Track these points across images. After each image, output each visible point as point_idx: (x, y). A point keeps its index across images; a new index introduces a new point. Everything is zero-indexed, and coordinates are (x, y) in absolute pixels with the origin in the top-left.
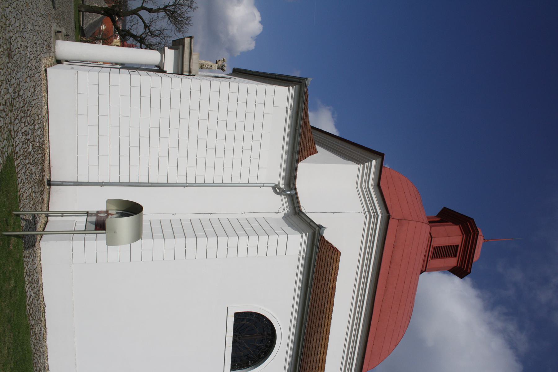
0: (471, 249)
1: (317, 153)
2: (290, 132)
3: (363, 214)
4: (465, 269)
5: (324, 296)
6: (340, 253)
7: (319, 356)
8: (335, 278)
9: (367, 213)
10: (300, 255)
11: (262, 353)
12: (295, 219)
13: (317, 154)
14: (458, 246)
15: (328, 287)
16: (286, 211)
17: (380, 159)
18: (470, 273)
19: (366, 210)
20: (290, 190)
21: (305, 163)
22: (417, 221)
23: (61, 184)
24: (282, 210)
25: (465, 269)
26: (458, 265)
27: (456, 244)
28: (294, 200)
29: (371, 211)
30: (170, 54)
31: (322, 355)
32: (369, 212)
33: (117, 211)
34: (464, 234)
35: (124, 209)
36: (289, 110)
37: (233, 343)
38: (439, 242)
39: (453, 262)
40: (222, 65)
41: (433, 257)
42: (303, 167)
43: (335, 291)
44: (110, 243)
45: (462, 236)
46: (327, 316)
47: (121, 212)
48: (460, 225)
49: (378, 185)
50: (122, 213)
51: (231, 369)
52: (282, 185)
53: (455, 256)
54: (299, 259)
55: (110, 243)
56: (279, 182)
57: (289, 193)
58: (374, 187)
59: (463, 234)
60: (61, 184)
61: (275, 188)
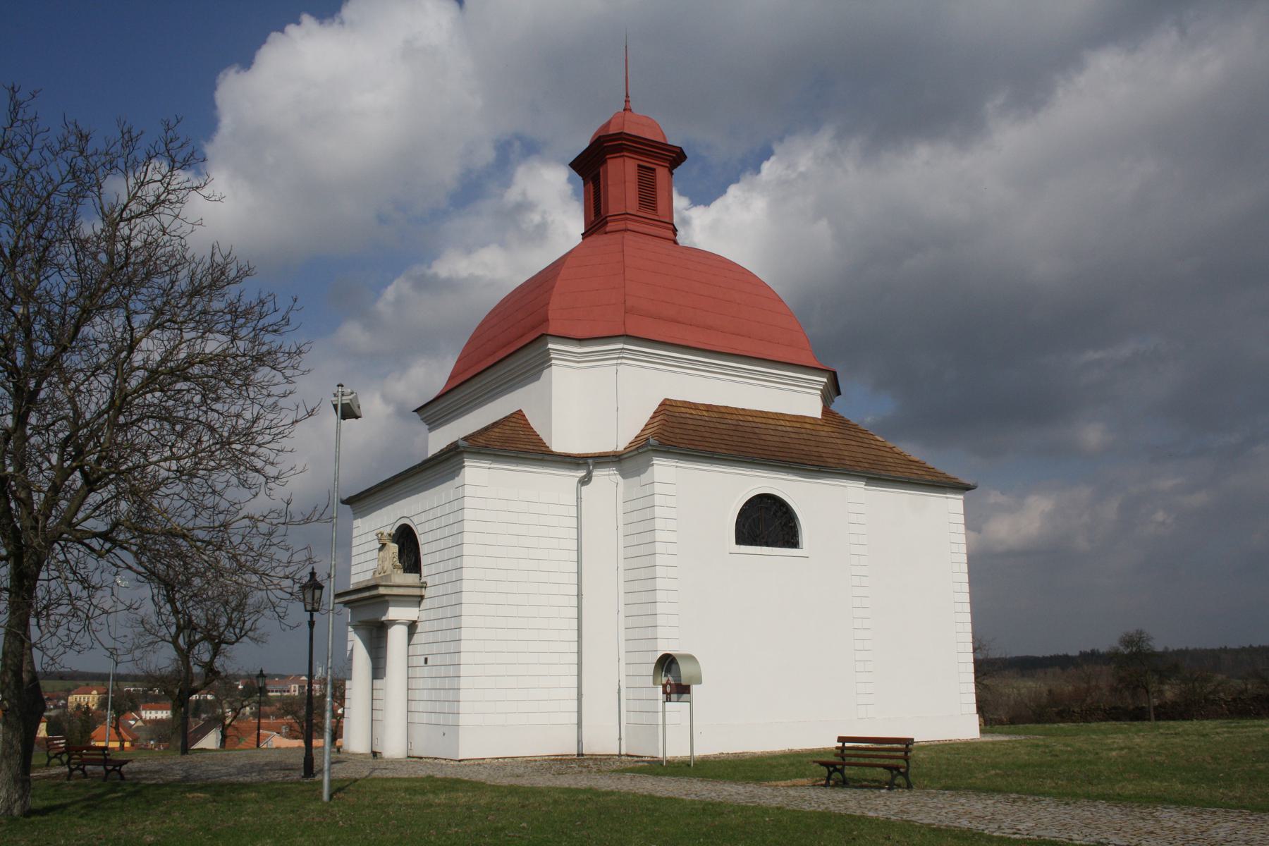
0: (646, 145)
1: (520, 411)
2: (517, 464)
3: (619, 368)
4: (674, 155)
5: (719, 426)
6: (666, 400)
7: (788, 428)
8: (695, 406)
9: (619, 361)
10: (677, 467)
11: (781, 510)
12: (627, 465)
13: (525, 412)
14: (639, 166)
15: (707, 419)
16: (616, 472)
17: (549, 338)
18: (681, 148)
19: (615, 362)
20: (587, 464)
21: (550, 439)
22: (624, 280)
23: (580, 742)
24: (613, 478)
25: (674, 155)
26: (668, 165)
27: (637, 168)
28: (602, 460)
29: (618, 356)
30: (394, 613)
31: (788, 424)
32: (618, 358)
33: (663, 675)
34: (622, 154)
35: (660, 670)
36: (492, 466)
37: (768, 545)
38: (632, 204)
39: (661, 173)
40: (389, 538)
41: (654, 209)
42: (557, 447)
43: (710, 406)
44: (699, 681)
45: (625, 158)
46: (741, 418)
47: (663, 673)
48: (608, 156)
49: (581, 341)
50: (665, 672)
51: (796, 548)
52: (582, 473)
53: (654, 170)
54: (680, 467)
55: (699, 681)
56: (574, 476)
57: (591, 467)
58: (581, 346)
59: (623, 156)
60: (580, 742)
61: (585, 481)
